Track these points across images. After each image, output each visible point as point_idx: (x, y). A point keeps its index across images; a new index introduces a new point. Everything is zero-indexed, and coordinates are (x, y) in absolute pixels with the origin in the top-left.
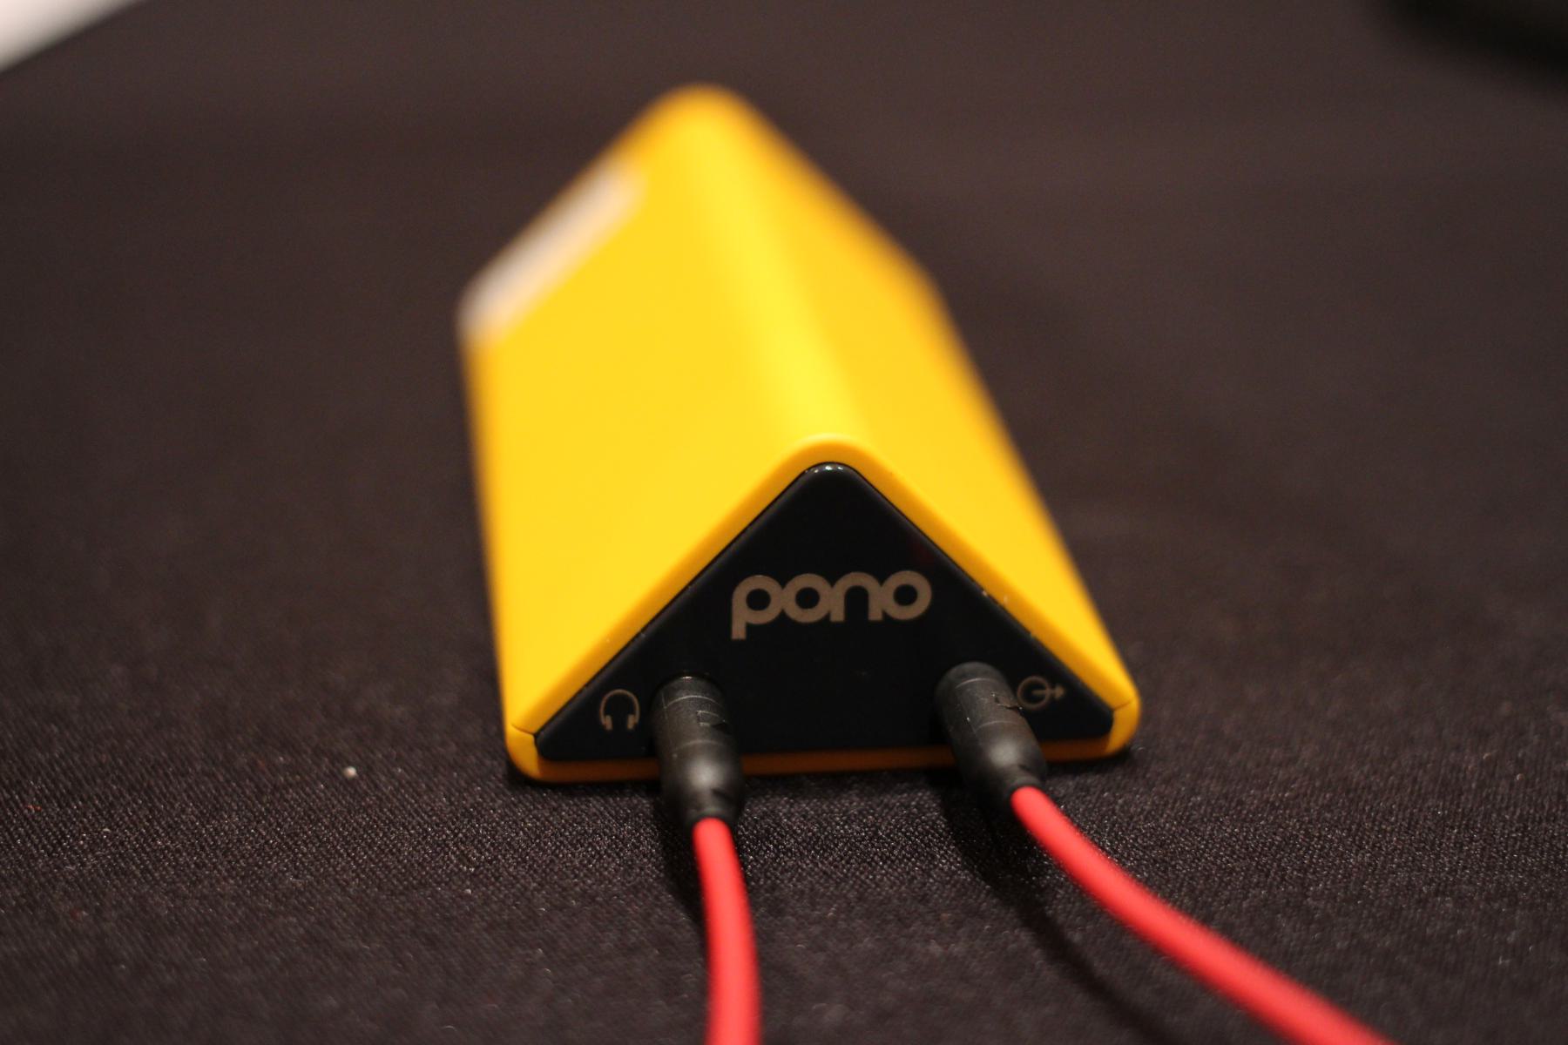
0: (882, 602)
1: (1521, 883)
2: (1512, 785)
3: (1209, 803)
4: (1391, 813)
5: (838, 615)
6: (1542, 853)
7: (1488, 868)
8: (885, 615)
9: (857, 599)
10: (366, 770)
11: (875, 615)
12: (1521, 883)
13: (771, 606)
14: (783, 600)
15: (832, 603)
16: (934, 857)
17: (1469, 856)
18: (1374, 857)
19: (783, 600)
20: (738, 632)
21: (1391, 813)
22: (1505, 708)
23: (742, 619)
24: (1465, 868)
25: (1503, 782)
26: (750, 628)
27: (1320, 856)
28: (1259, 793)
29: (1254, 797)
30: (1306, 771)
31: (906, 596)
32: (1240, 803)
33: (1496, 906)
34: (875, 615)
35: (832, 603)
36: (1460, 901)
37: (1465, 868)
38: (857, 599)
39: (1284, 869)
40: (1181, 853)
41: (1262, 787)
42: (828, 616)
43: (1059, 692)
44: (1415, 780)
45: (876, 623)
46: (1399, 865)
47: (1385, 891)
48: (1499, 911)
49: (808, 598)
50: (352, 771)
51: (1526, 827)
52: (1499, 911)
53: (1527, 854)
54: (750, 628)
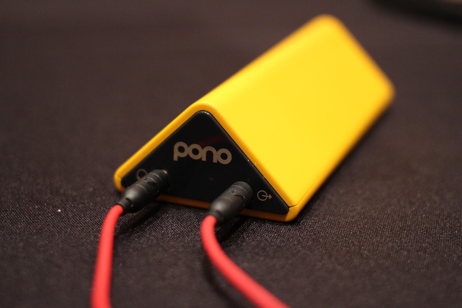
0: (217, 157)
1: (427, 247)
2: (422, 218)
3: (329, 223)
4: (386, 226)
5: (204, 159)
6: (433, 238)
7: (416, 242)
8: (218, 161)
9: (210, 155)
10: (64, 209)
11: (215, 161)
12: (427, 247)
13: (185, 152)
14: (188, 151)
15: (202, 155)
16: (244, 238)
17: (410, 238)
18: (381, 238)
19: (188, 151)
20: (175, 158)
21: (386, 226)
22: (419, 195)
23: (177, 155)
24: (409, 242)
25: (420, 217)
26: (179, 158)
27: (364, 238)
28: (345, 220)
29: (343, 221)
30: (359, 213)
31: (224, 156)
32: (339, 222)
33: (420, 253)
34: (215, 161)
35: (202, 155)
36: (409, 251)
37: (409, 242)
38: (210, 155)
39: (354, 242)
40: (321, 237)
41: (345, 218)
42: (201, 159)
43: (270, 197)
44: (392, 216)
45: (215, 163)
46: (389, 241)
47: (385, 249)
48: (421, 255)
49: (195, 152)
50: (59, 211)
51: (427, 230)
52: (421, 255)
53: (428, 238)
54: (179, 158)
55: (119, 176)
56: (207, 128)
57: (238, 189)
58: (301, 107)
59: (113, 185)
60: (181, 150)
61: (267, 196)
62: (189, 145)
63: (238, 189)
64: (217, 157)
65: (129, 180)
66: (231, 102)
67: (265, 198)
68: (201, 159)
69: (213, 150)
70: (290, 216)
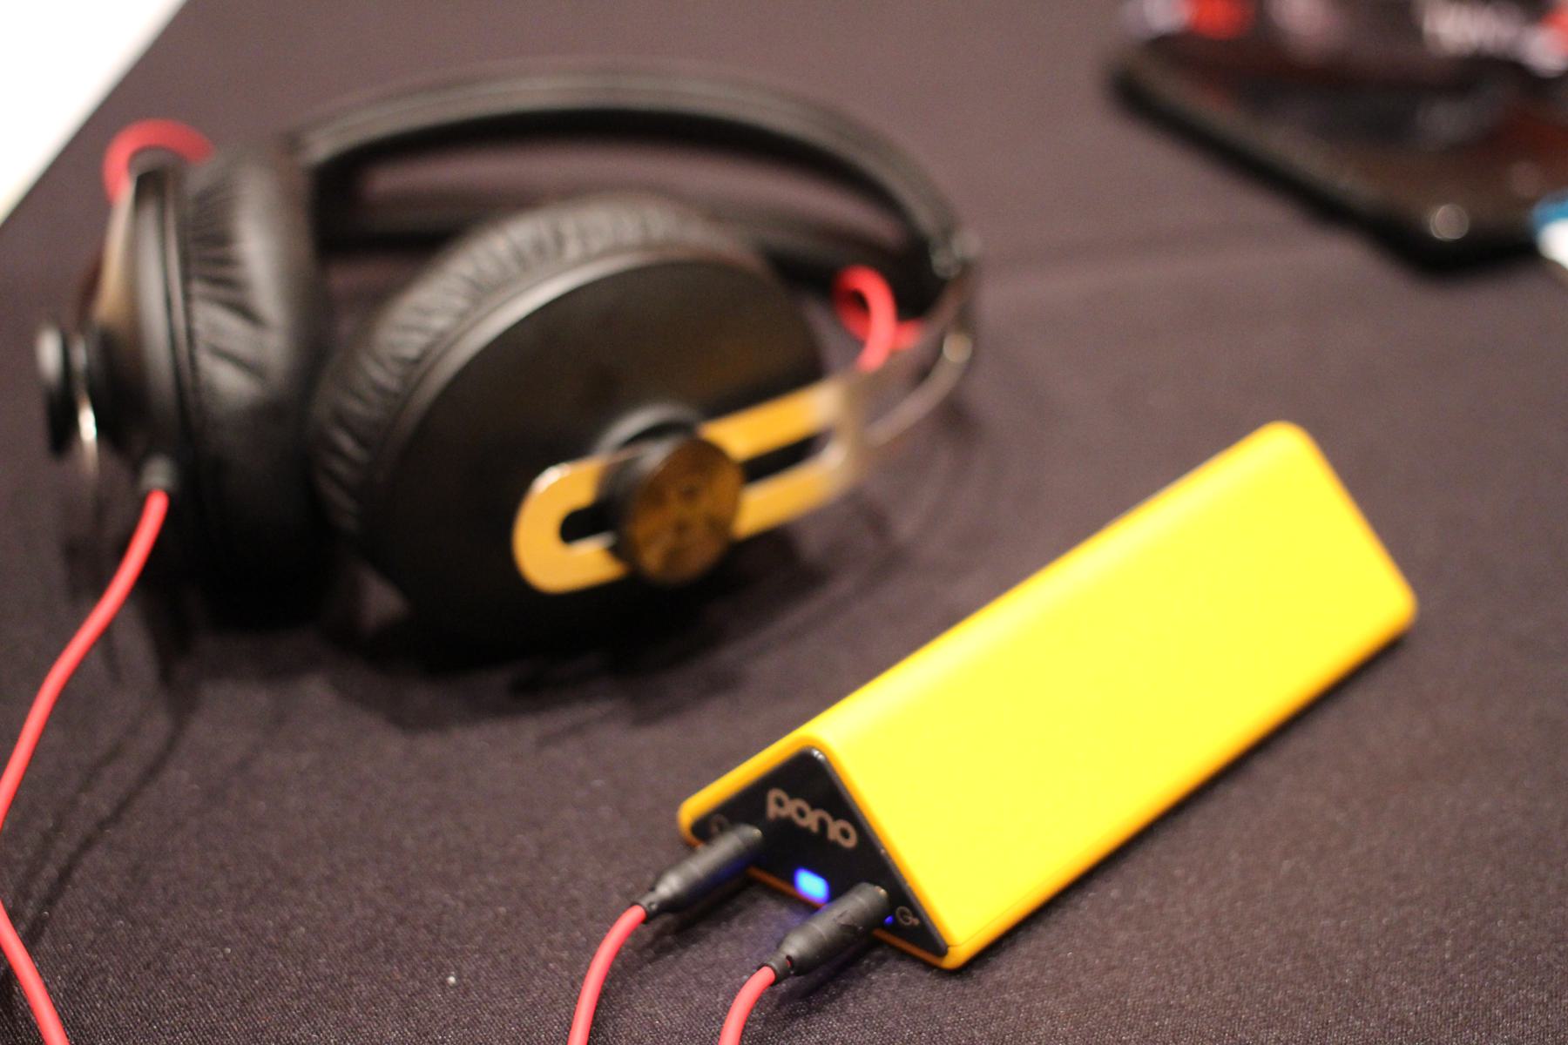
9: (823, 824)
14: (791, 808)
15: (811, 820)
19: (791, 808)
23: (773, 810)
38: (823, 824)
43: (916, 922)
56: (811, 776)
57: (864, 899)
59: (673, 819)
60: (780, 803)
63: (864, 899)
65: (705, 829)
69: (828, 819)
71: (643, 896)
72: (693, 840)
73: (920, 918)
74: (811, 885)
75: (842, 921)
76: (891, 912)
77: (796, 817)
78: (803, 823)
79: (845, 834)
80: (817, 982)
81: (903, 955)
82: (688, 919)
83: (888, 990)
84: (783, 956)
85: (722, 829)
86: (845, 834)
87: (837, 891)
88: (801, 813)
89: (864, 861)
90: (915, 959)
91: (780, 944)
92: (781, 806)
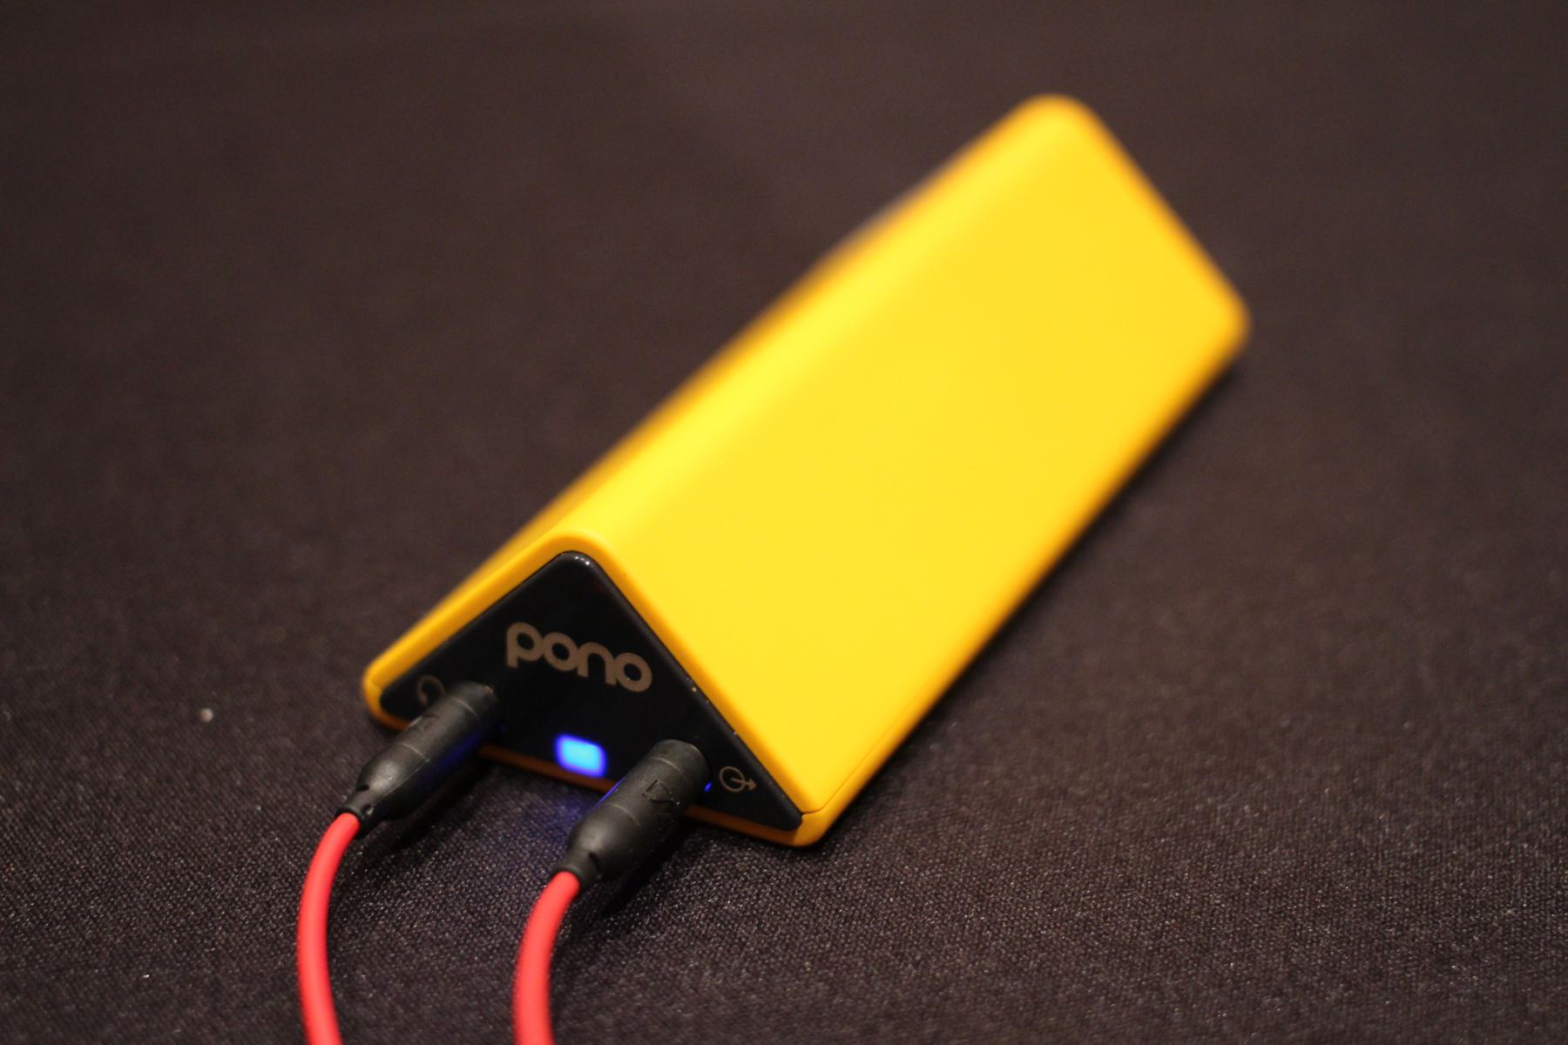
5: (583, 672)
9: (596, 663)
11: (610, 679)
14: (543, 647)
15: (577, 661)
19: (543, 647)
23: (514, 654)
26: (520, 661)
34: (610, 679)
38: (596, 663)
43: (752, 785)
54: (520, 661)
55: (375, 683)
56: (579, 594)
57: (670, 763)
58: (886, 460)
59: (356, 690)
60: (525, 642)
61: (743, 782)
62: (542, 660)
63: (670, 763)
64: (614, 671)
65: (406, 697)
66: (637, 514)
67: (738, 785)
68: (574, 672)
69: (605, 654)
70: (807, 833)
71: (351, 798)
72: (386, 718)
73: (758, 780)
74: (581, 755)
75: (653, 796)
76: (711, 774)
77: (551, 659)
78: (564, 666)
79: (632, 672)
80: (618, 894)
81: (741, 840)
82: (404, 834)
83: (722, 888)
84: (584, 855)
85: (434, 696)
86: (632, 672)
87: (619, 765)
88: (561, 652)
89: (665, 705)
90: (758, 842)
91: (571, 842)
92: (527, 646)
